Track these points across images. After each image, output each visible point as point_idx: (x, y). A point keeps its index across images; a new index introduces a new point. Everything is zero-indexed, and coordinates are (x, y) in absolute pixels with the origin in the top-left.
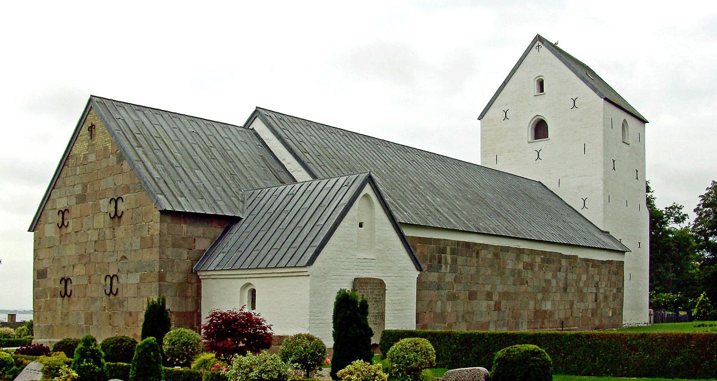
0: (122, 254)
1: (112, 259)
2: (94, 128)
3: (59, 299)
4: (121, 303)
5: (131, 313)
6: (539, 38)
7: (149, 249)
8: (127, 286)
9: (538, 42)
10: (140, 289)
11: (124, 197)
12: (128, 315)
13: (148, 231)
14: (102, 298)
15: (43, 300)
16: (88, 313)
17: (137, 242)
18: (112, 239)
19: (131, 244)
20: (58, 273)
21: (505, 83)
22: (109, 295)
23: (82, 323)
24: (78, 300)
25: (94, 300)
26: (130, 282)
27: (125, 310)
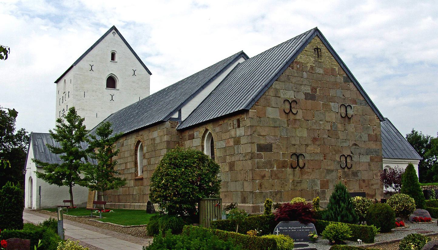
0: (353, 142)
1: (345, 145)
2: (320, 51)
3: (289, 170)
4: (355, 174)
5: (364, 181)
6: (114, 28)
7: (375, 142)
8: (360, 163)
9: (114, 30)
10: (370, 165)
11: (352, 106)
12: (361, 182)
13: (373, 131)
14: (337, 170)
15: (267, 170)
16: (324, 181)
17: (365, 137)
18: (343, 131)
19: (361, 137)
20: (287, 148)
21: (92, 48)
22: (344, 168)
23: (318, 188)
24: (313, 171)
25: (329, 171)
26: (362, 161)
27: (359, 178)
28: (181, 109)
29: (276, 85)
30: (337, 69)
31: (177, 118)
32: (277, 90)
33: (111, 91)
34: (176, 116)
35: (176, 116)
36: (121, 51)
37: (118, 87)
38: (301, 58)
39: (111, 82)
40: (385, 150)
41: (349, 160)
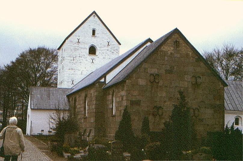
6: (94, 12)
28: (106, 77)
29: (145, 65)
30: (191, 53)
31: (103, 82)
32: (145, 69)
33: (93, 56)
34: (103, 80)
35: (103, 80)
36: (100, 29)
37: (97, 54)
38: (165, 48)
39: (92, 50)
40: (229, 103)
41: (196, 112)
